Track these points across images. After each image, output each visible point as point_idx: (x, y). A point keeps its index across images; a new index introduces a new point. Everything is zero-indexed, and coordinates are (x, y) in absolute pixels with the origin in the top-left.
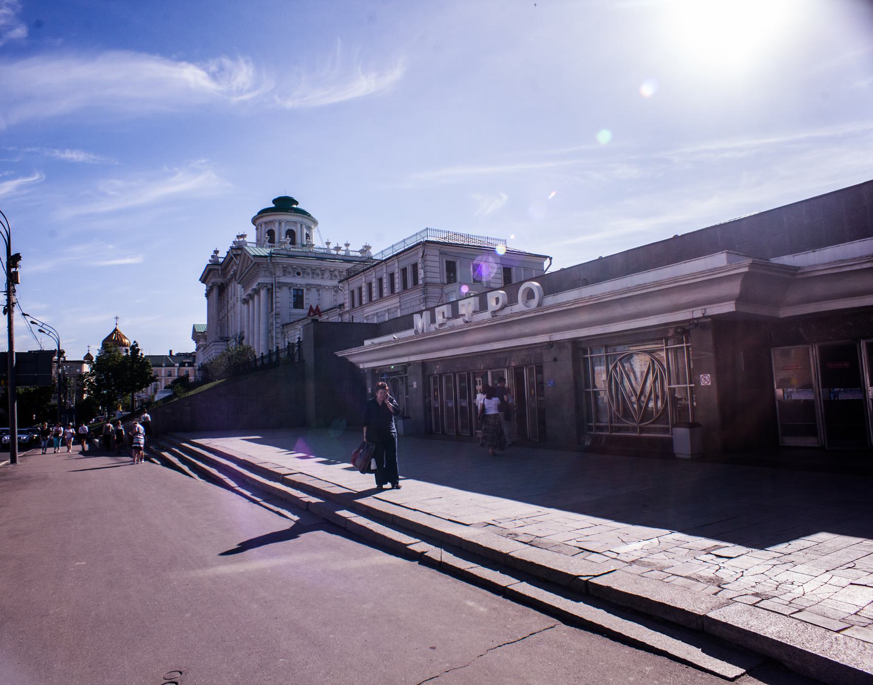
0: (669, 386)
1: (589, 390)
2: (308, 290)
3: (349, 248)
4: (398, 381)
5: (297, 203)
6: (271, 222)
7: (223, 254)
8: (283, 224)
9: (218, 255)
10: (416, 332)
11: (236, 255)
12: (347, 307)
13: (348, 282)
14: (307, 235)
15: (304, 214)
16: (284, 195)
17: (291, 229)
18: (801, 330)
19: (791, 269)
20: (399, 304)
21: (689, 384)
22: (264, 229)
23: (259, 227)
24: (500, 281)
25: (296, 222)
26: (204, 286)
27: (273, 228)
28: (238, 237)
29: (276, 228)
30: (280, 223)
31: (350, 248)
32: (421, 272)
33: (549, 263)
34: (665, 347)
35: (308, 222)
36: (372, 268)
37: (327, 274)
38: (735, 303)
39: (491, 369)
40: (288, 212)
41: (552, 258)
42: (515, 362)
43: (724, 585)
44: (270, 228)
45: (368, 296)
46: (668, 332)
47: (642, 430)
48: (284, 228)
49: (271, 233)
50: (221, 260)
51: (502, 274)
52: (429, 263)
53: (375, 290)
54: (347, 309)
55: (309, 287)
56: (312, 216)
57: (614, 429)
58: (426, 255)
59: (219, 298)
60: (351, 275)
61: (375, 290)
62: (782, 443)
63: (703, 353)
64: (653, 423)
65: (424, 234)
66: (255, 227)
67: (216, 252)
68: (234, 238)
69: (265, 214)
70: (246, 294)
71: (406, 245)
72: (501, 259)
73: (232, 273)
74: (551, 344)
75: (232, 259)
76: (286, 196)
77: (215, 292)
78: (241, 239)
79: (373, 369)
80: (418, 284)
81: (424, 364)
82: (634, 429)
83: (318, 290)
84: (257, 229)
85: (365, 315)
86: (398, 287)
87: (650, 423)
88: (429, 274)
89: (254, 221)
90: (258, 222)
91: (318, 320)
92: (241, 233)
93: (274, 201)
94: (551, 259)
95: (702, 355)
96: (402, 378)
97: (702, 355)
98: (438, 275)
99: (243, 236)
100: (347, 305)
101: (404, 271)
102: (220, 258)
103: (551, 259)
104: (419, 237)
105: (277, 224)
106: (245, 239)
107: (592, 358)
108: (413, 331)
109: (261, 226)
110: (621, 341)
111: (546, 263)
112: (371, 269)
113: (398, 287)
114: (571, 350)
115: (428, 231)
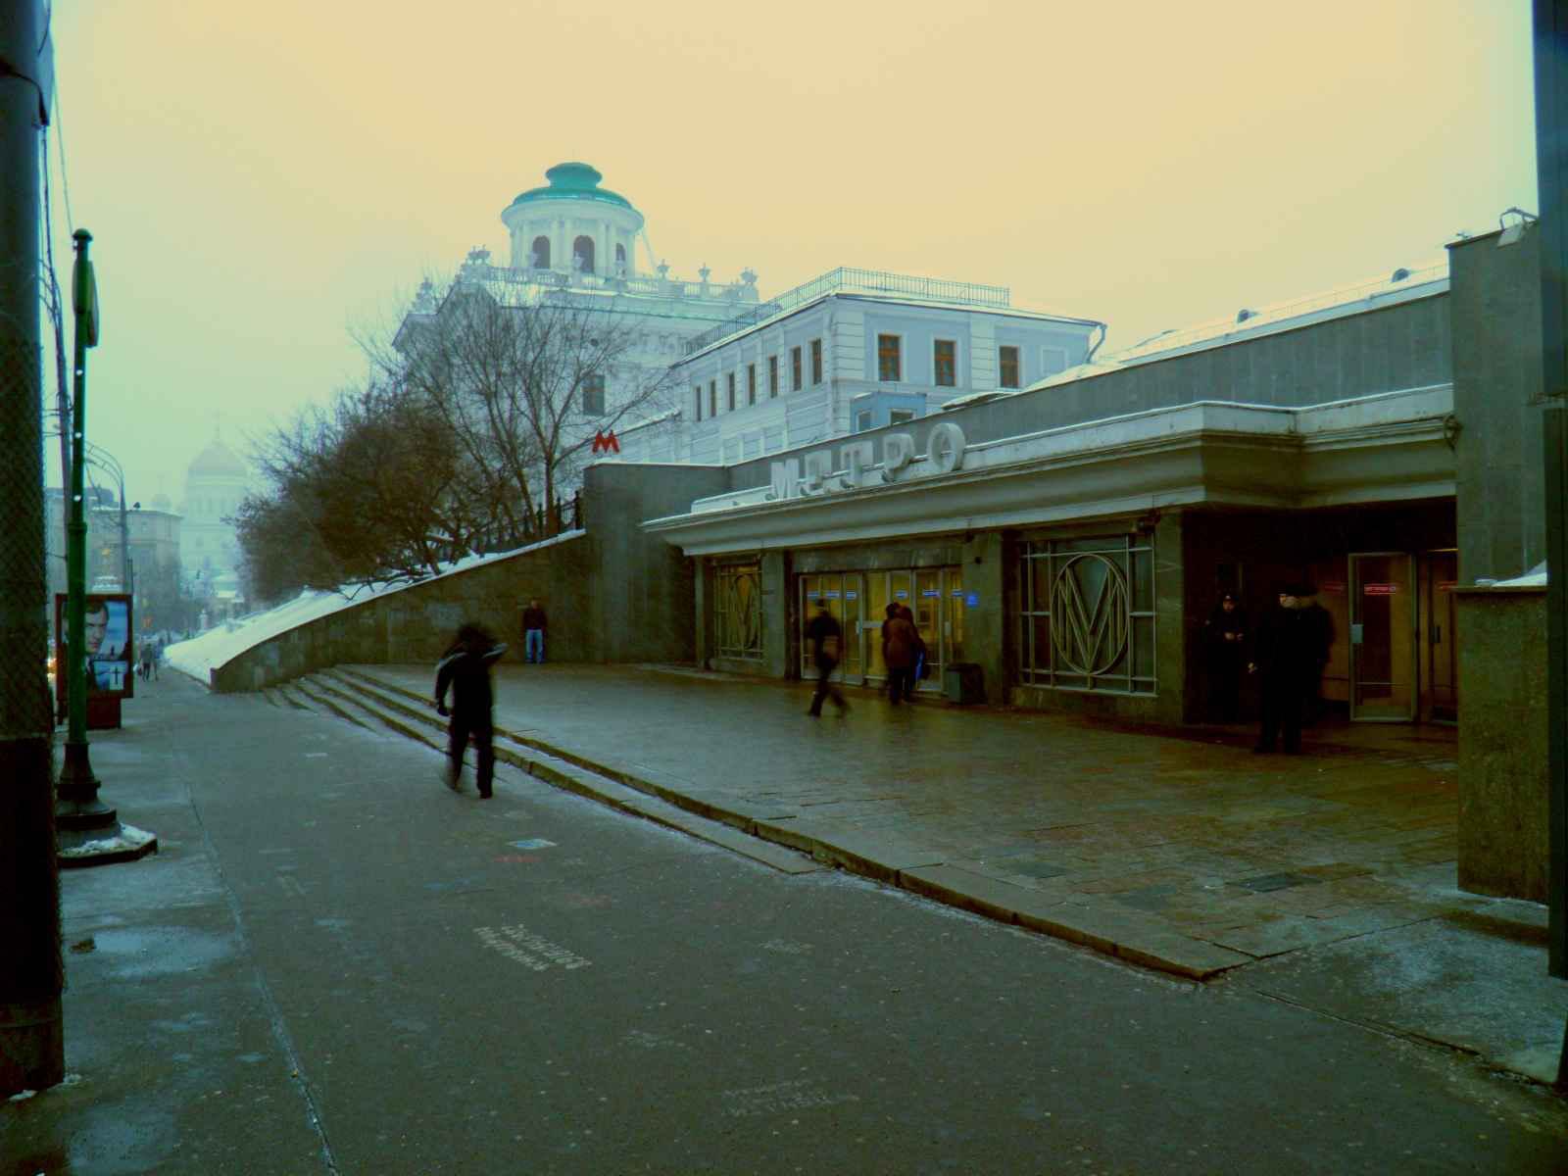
5: (597, 177)
19: (1042, 476)
22: (528, 239)
23: (518, 232)
32: (826, 356)
37: (653, 341)
43: (1236, 963)
47: (1095, 683)
48: (571, 235)
49: (541, 246)
53: (741, 386)
56: (635, 206)
58: (836, 324)
61: (741, 386)
64: (1105, 673)
65: (835, 280)
66: (509, 231)
68: (463, 258)
74: (969, 535)
79: (708, 559)
81: (788, 554)
82: (1082, 681)
84: (512, 235)
87: (1105, 673)
88: (841, 363)
89: (506, 217)
93: (551, 173)
94: (1104, 327)
98: (861, 365)
103: (1104, 327)
104: (825, 285)
105: (555, 225)
107: (1034, 560)
109: (521, 229)
111: (1095, 335)
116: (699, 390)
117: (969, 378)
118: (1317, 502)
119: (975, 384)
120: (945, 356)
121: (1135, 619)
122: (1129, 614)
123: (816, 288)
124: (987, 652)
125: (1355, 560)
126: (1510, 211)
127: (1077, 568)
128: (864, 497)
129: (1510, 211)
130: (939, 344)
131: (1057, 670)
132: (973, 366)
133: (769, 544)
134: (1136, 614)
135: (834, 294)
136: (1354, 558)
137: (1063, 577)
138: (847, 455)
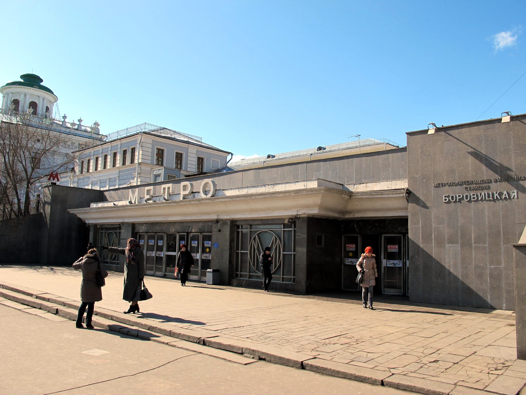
0: (283, 252)
1: (238, 251)
3: (81, 123)
4: (114, 234)
5: (42, 81)
10: (130, 202)
14: (47, 109)
18: (355, 226)
21: (293, 252)
25: (39, 96)
31: (82, 124)
33: (231, 158)
34: (282, 229)
35: (50, 98)
38: (319, 209)
39: (178, 233)
40: (33, 87)
41: (233, 154)
42: (195, 230)
46: (285, 220)
51: (197, 165)
57: (284, 279)
59: (267, 361)
62: (384, 292)
63: (301, 235)
66: (2, 95)
71: (128, 132)
72: (197, 151)
76: (33, 74)
91: (56, 183)
93: (22, 77)
94: (232, 155)
95: (301, 236)
96: (116, 233)
97: (301, 236)
103: (232, 155)
105: (22, 96)
108: (128, 201)
110: (259, 223)
111: (229, 157)
114: (229, 225)
116: (83, 162)
117: (186, 167)
118: (351, 216)
119: (189, 169)
120: (179, 157)
121: (284, 255)
122: (282, 253)
123: (135, 129)
124: (224, 264)
125: (385, 237)
126: (433, 124)
127: (259, 235)
128: (109, 209)
129: (433, 124)
130: (177, 154)
131: (166, 272)
132: (188, 163)
133: (126, 221)
134: (284, 253)
135: (142, 131)
136: (385, 237)
137: (254, 239)
138: (165, 188)
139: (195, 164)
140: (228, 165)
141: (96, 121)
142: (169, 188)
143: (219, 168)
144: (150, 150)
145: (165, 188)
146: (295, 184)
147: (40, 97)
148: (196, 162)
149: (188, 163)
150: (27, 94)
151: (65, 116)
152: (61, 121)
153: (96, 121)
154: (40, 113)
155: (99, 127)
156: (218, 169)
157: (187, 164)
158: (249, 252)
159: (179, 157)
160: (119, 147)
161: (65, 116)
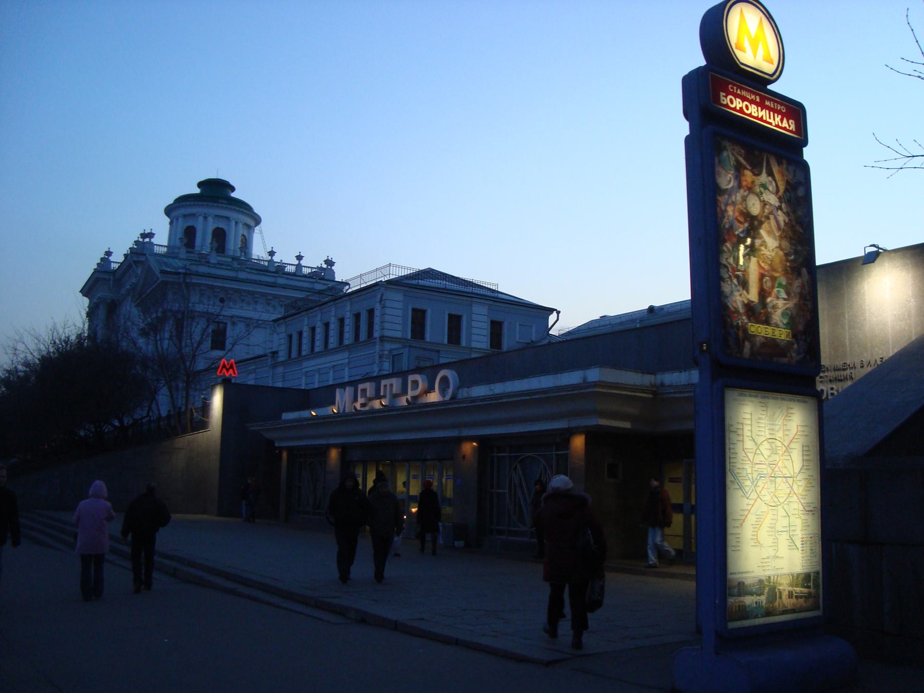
2: (234, 324)
5: (233, 189)
6: (193, 215)
7: (118, 258)
8: (210, 219)
9: (110, 258)
11: (136, 263)
12: (282, 356)
13: (286, 322)
15: (241, 207)
16: (216, 178)
17: (220, 227)
20: (347, 360)
22: (182, 225)
23: (175, 220)
24: (485, 339)
26: (86, 301)
27: (195, 225)
28: (144, 236)
29: (199, 225)
30: (205, 218)
31: (303, 263)
33: (556, 319)
36: (318, 308)
44: (190, 224)
45: (310, 344)
50: (115, 266)
52: (388, 311)
53: (319, 336)
54: (281, 359)
55: (234, 320)
60: (296, 309)
61: (319, 336)
67: (109, 253)
68: (136, 236)
69: (184, 204)
70: (146, 322)
73: (128, 287)
75: (130, 266)
77: (102, 313)
78: (147, 240)
80: (373, 337)
83: (248, 325)
84: (171, 223)
85: (304, 370)
86: (348, 338)
88: (387, 325)
89: (169, 211)
90: (174, 214)
92: (147, 231)
93: (200, 185)
94: (558, 312)
98: (399, 327)
99: (151, 235)
100: (281, 354)
101: (357, 316)
102: (114, 262)
103: (558, 312)
104: (379, 274)
106: (153, 240)
109: (177, 219)
111: (552, 318)
112: (315, 309)
113: (348, 338)
115: (391, 267)
120: (455, 322)
128: (295, 424)
138: (385, 386)
139: (485, 334)
140: (551, 332)
141: (328, 257)
142: (391, 385)
143: (534, 339)
144: (400, 313)
145: (385, 386)
146: (882, 358)
147: (231, 219)
148: (487, 329)
149: (472, 333)
150: (209, 216)
151: (272, 250)
152: (266, 261)
153: (328, 257)
154: (232, 248)
155: (333, 268)
156: (532, 341)
157: (470, 334)
158: (507, 491)
159: (455, 322)
160: (332, 315)
161: (272, 250)
